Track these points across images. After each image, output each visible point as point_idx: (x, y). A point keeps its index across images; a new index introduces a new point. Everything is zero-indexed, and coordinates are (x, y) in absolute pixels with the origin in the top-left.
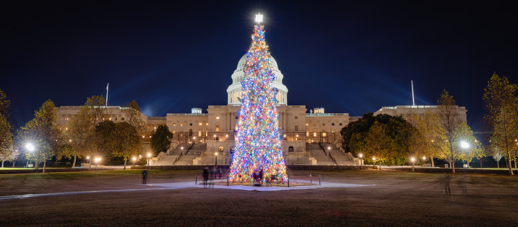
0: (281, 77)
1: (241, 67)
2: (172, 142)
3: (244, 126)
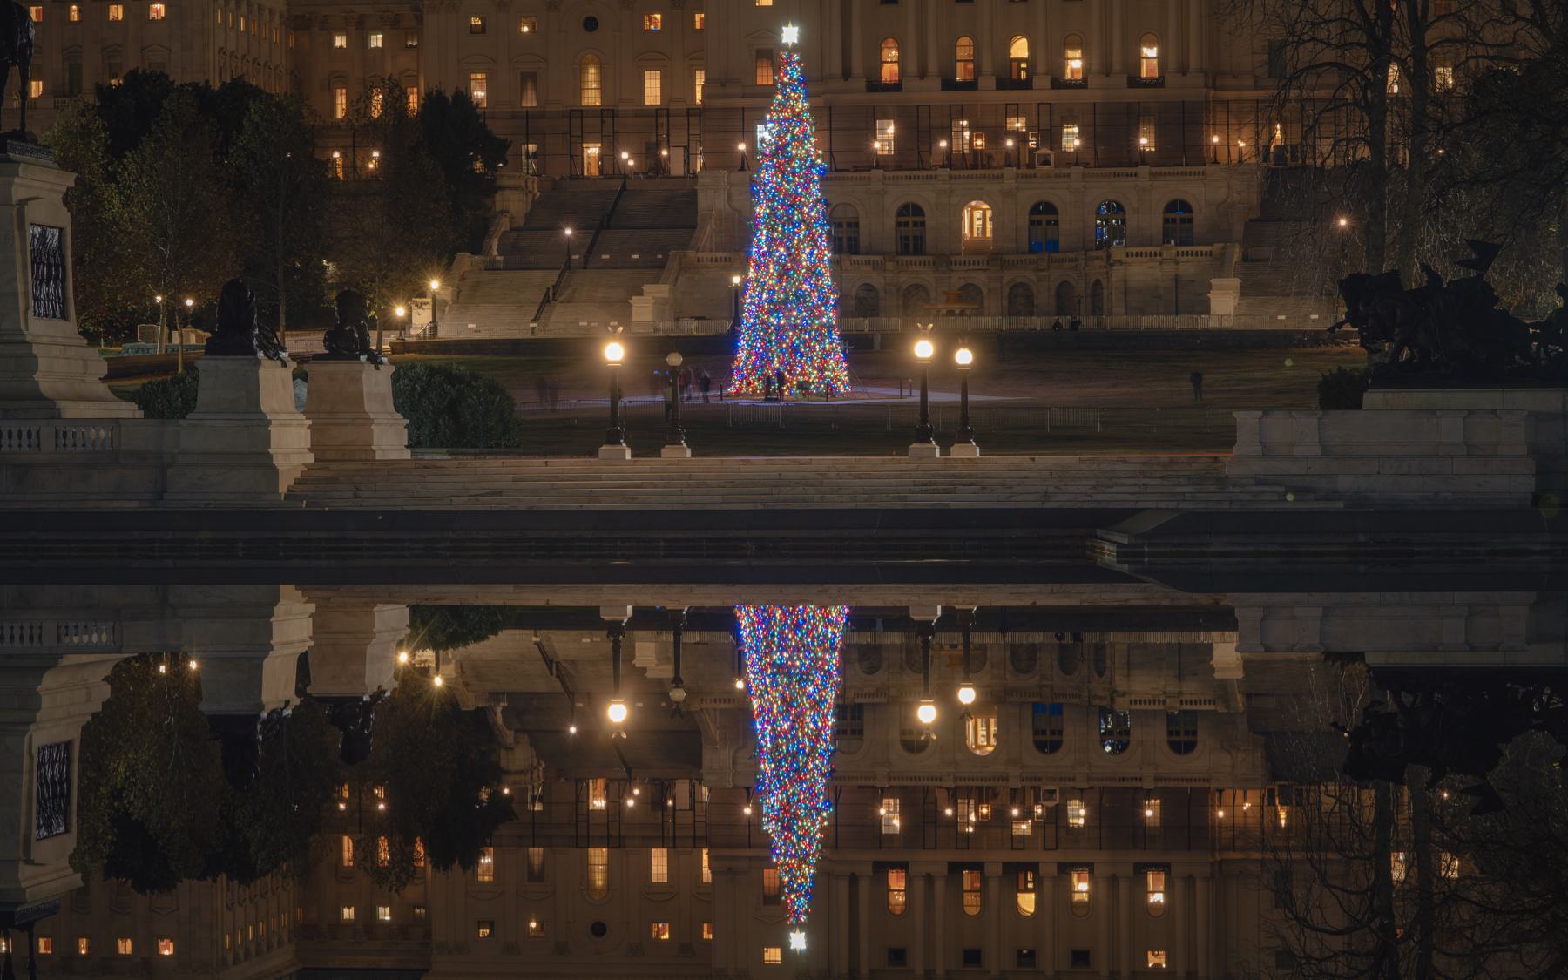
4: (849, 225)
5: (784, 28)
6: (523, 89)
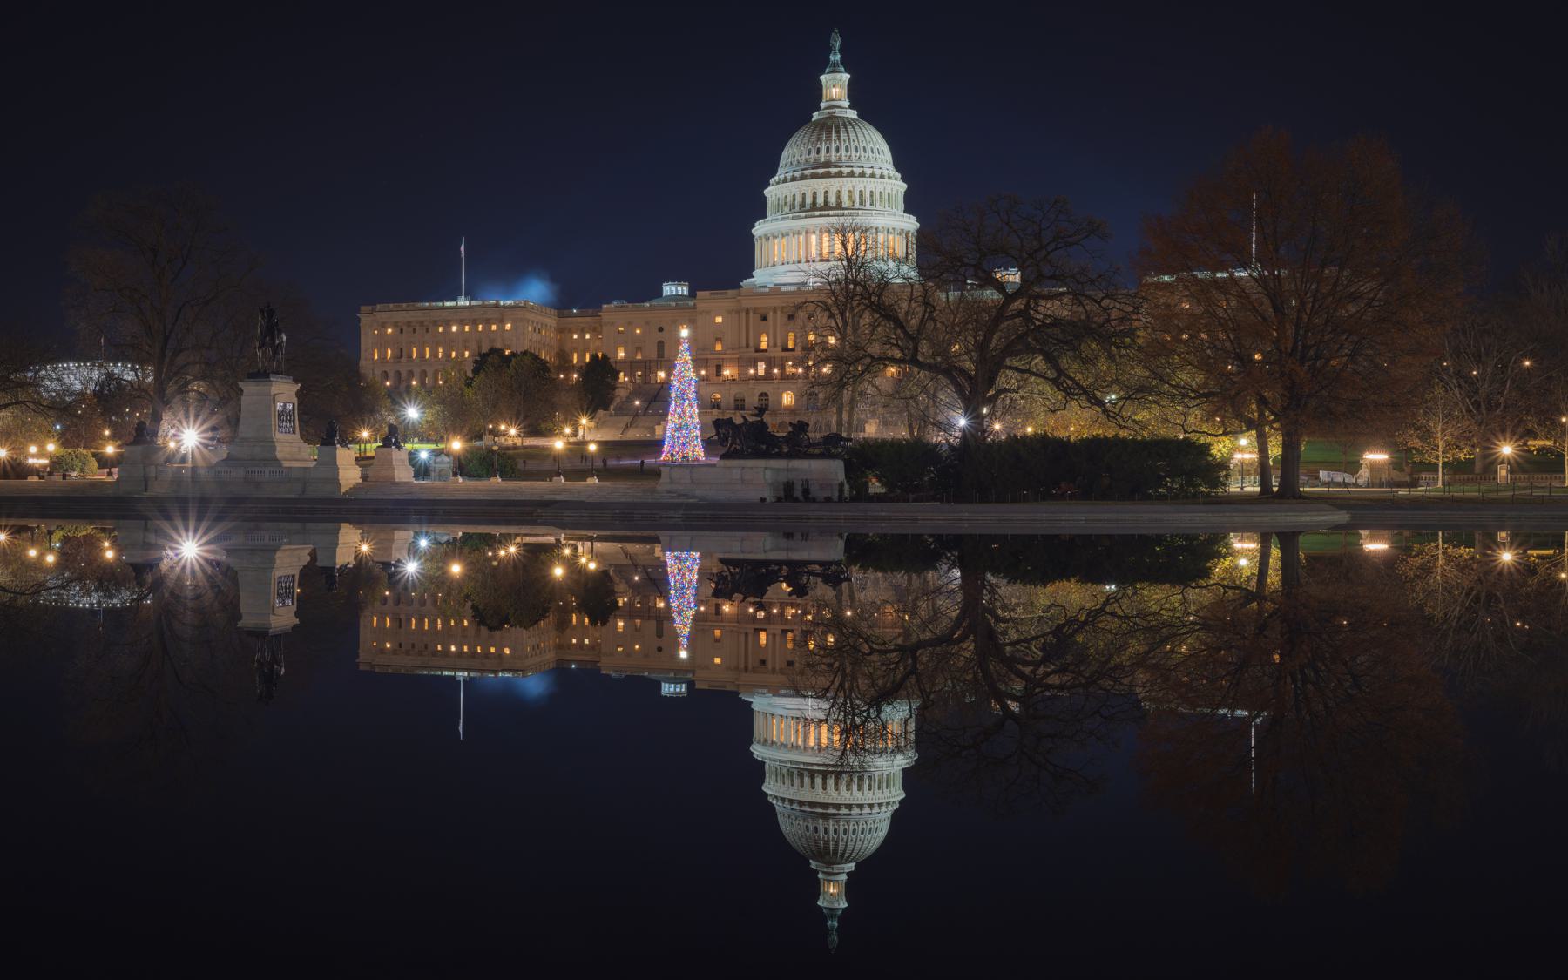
6: (637, 352)
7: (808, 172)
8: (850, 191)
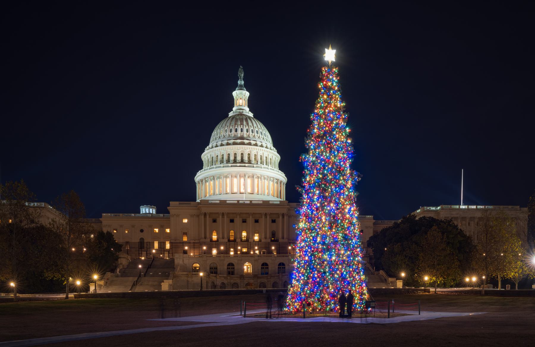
0: (277, 158)
1: (216, 141)
2: (120, 258)
3: (312, 230)
4: (215, 268)
5: (326, 50)
7: (231, 141)
8: (255, 155)
